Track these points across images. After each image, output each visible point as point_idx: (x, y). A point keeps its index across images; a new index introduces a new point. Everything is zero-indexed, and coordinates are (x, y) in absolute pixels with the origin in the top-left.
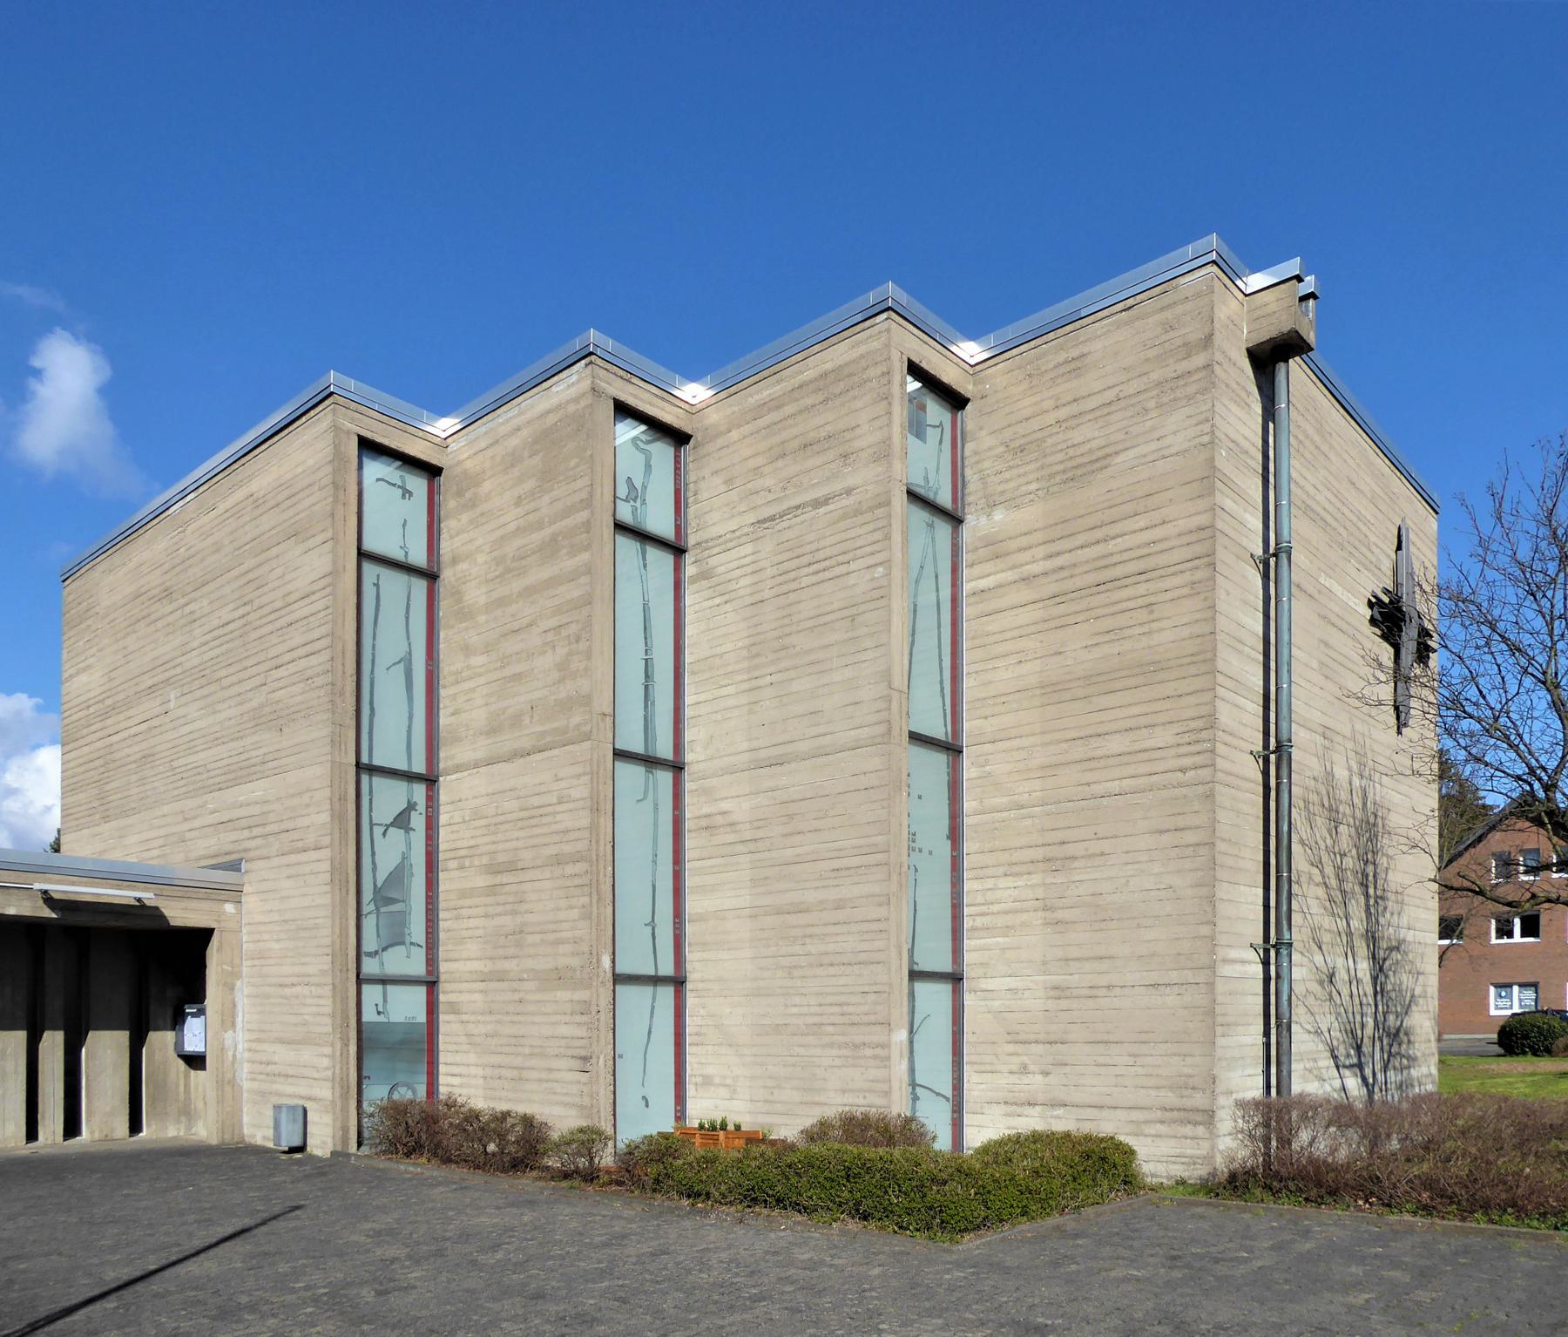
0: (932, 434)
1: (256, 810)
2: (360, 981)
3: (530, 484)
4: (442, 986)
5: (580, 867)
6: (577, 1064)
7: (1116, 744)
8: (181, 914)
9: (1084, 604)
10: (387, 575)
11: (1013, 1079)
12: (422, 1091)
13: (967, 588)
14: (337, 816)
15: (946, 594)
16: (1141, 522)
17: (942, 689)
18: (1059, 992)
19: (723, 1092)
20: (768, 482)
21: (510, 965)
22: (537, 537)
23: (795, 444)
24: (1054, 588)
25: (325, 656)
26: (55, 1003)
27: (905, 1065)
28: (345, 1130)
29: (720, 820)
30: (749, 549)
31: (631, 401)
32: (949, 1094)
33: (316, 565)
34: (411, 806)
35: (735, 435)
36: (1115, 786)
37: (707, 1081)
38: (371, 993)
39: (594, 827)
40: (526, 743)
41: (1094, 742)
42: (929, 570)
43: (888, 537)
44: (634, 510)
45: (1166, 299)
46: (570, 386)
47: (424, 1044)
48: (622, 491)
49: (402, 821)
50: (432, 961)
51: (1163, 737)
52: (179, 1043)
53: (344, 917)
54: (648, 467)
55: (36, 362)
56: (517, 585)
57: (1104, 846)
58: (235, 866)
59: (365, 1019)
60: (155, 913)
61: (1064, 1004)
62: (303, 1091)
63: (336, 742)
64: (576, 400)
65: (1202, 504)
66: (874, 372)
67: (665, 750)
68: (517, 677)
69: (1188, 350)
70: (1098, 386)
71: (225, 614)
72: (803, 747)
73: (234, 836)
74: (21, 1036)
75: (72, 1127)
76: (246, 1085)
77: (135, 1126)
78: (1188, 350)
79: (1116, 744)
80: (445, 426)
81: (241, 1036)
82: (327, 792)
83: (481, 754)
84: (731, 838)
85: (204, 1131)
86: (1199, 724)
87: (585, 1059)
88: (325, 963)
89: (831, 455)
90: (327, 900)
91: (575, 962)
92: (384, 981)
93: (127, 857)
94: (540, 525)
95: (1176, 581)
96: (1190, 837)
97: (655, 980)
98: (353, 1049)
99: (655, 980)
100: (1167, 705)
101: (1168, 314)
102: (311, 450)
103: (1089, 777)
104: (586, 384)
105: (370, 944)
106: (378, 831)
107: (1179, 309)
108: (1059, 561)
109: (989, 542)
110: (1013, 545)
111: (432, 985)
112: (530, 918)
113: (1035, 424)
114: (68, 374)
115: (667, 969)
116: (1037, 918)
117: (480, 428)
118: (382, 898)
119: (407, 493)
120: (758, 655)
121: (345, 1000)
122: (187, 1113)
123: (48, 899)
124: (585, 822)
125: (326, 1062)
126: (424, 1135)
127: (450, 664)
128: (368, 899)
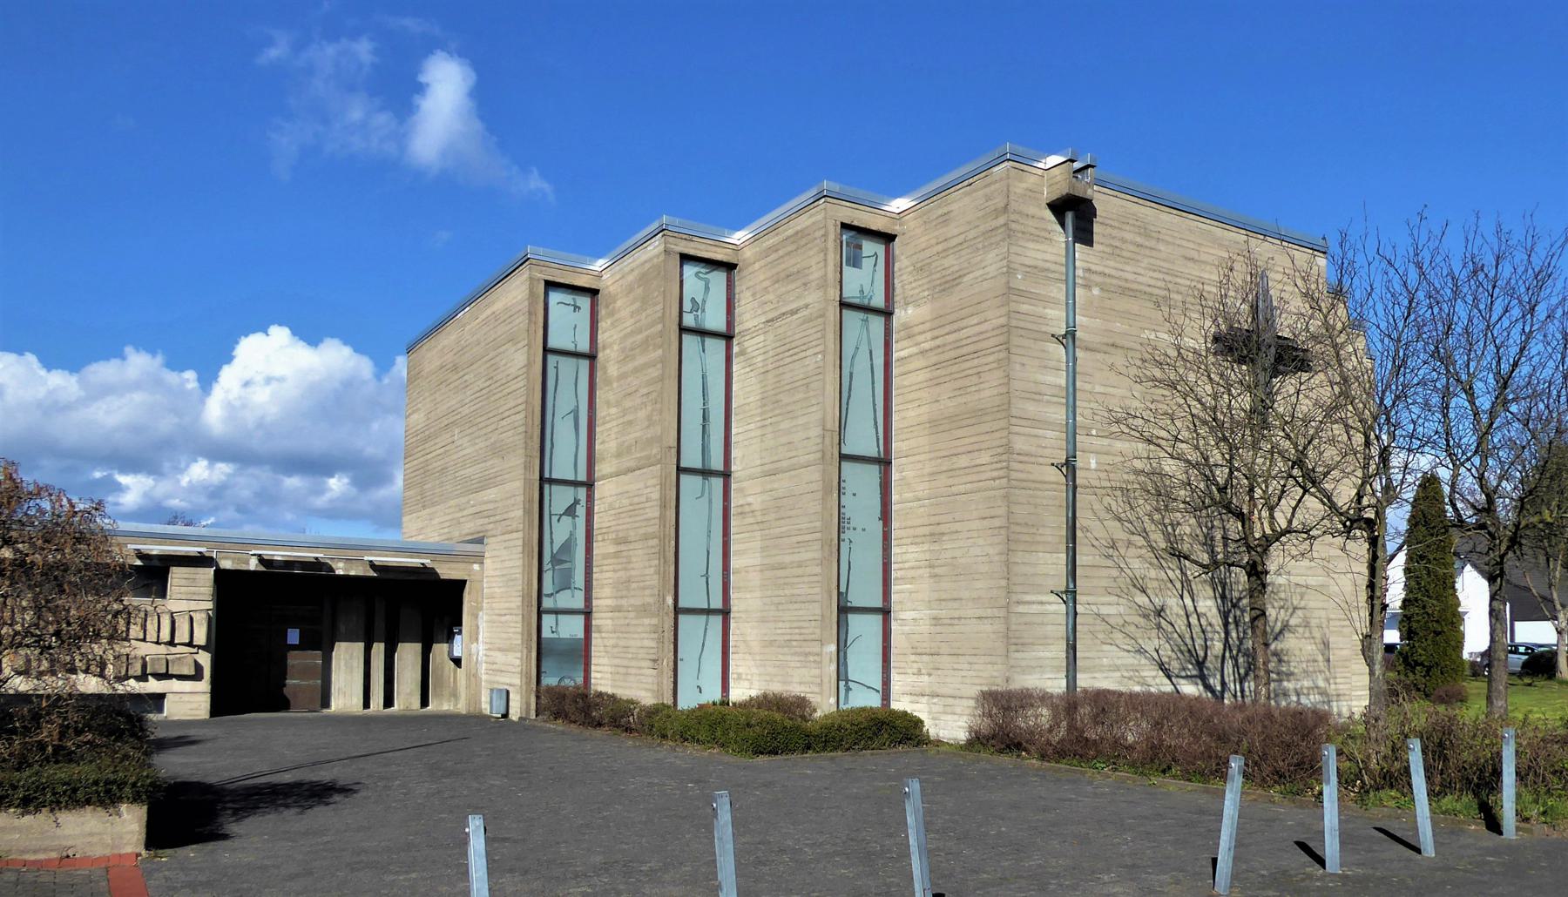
0: (867, 264)
1: (491, 506)
3: (637, 305)
4: (595, 615)
5: (655, 542)
6: (650, 664)
7: (963, 461)
8: (447, 572)
9: (949, 370)
10: (562, 360)
11: (914, 678)
12: (580, 681)
13: (895, 356)
14: (527, 512)
15: (879, 361)
16: (975, 320)
18: (936, 621)
19: (746, 684)
20: (771, 297)
21: (624, 602)
22: (640, 337)
23: (782, 275)
24: (934, 359)
25: (522, 415)
26: (380, 625)
28: (528, 704)
29: (747, 509)
30: (762, 338)
31: (692, 252)
33: (519, 359)
34: (577, 502)
35: (757, 266)
36: (962, 488)
37: (739, 677)
38: (548, 620)
39: (662, 517)
40: (632, 464)
41: (955, 459)
42: (864, 349)
43: (823, 337)
44: (696, 317)
45: (988, 180)
46: (655, 247)
47: (582, 652)
48: (687, 306)
49: (570, 511)
51: (985, 458)
52: (451, 651)
53: (530, 573)
54: (707, 288)
55: (422, 79)
56: (630, 366)
57: (957, 526)
58: (480, 541)
60: (432, 572)
61: (939, 629)
62: (507, 680)
63: (527, 467)
64: (658, 256)
65: (1004, 310)
66: (819, 234)
67: (717, 463)
68: (630, 423)
69: (997, 213)
70: (956, 232)
71: (481, 384)
72: (785, 464)
73: (481, 521)
74: (361, 645)
75: (388, 702)
76: (484, 677)
77: (425, 702)
78: (997, 213)
79: (963, 461)
80: (599, 265)
81: (481, 647)
82: (521, 498)
83: (613, 470)
84: (751, 520)
85: (461, 707)
86: (1000, 450)
87: (655, 661)
88: (517, 602)
89: (799, 283)
90: (520, 563)
91: (651, 600)
92: (557, 612)
93: (415, 536)
94: (640, 331)
95: (991, 358)
96: (997, 522)
97: (708, 612)
98: (534, 654)
99: (708, 612)
100: (986, 437)
101: (987, 190)
102: (516, 293)
103: (951, 482)
104: (662, 248)
105: (548, 587)
106: (555, 519)
107: (993, 187)
108: (938, 342)
109: (906, 327)
110: (916, 330)
111: (587, 614)
112: (633, 573)
113: (927, 253)
114: (446, 86)
115: (717, 603)
116: (925, 572)
117: (616, 267)
118: (555, 560)
119: (577, 308)
121: (529, 624)
122: (455, 695)
123: (372, 565)
124: (657, 514)
125: (518, 662)
126: (574, 708)
127: (601, 412)
128: (544, 560)
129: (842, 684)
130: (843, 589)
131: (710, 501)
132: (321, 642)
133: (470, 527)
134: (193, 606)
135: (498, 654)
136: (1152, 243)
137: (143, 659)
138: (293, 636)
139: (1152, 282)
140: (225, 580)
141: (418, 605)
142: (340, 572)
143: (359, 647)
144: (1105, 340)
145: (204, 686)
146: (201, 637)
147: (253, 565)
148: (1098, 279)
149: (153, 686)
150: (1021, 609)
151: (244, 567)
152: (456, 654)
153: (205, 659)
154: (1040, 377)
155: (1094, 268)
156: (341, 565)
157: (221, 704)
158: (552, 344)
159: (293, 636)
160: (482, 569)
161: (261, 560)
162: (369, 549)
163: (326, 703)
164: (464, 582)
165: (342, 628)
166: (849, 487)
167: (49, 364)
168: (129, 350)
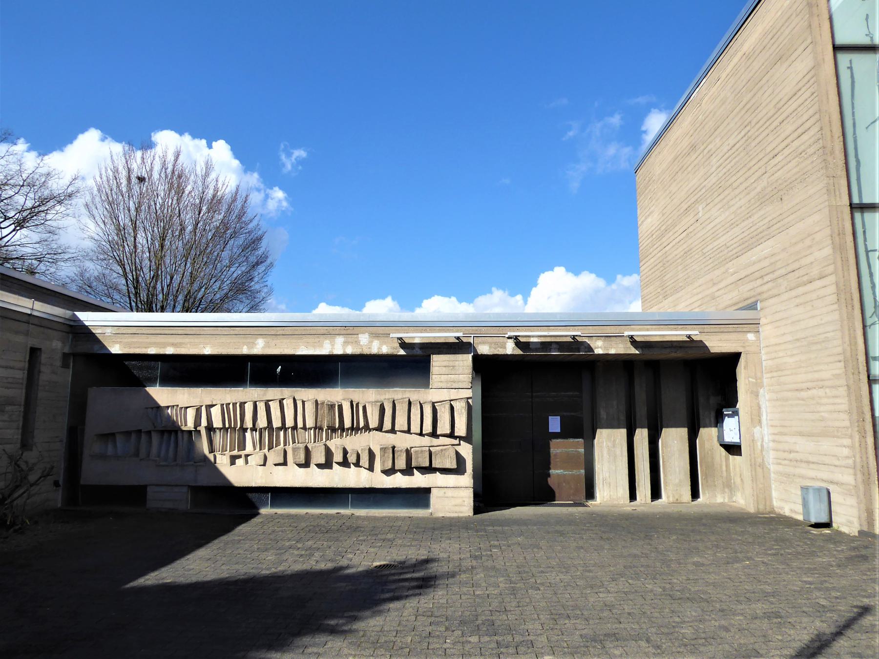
1: (766, 263)
14: (839, 248)
52: (721, 436)
53: (852, 328)
58: (753, 307)
60: (701, 345)
62: (825, 475)
63: (830, 191)
74: (623, 432)
75: (656, 493)
76: (772, 468)
77: (695, 494)
88: (838, 368)
121: (859, 399)
122: (729, 486)
123: (633, 342)
132: (582, 429)
133: (745, 291)
134: (454, 394)
135: (801, 440)
137: (408, 452)
138: (555, 424)
140: (487, 368)
141: (689, 384)
142: (598, 351)
143: (621, 434)
145: (466, 480)
146: (461, 429)
147: (510, 349)
149: (418, 480)
151: (501, 352)
152: (731, 437)
153: (466, 451)
156: (600, 343)
157: (486, 498)
159: (555, 424)
160: (758, 339)
161: (518, 344)
162: (628, 324)
163: (590, 494)
164: (740, 353)
165: (603, 414)
167: (460, 301)
168: (494, 289)
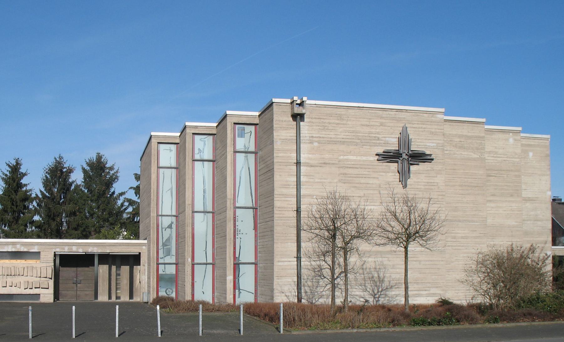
0: (247, 136)
2: (158, 264)
17: (251, 194)
27: (232, 296)
32: (254, 292)
34: (172, 223)
38: (161, 267)
49: (170, 227)
50: (177, 259)
54: (205, 144)
59: (160, 273)
77: (131, 297)
105: (161, 254)
118: (164, 245)
119: (171, 150)
120: (516, 176)
129: (237, 291)
130: (237, 256)
131: (207, 223)
134: (48, 265)
136: (344, 122)
139: (345, 137)
144: (321, 162)
148: (316, 139)
150: (280, 264)
154: (288, 179)
155: (314, 135)
158: (161, 165)
166: (239, 219)
